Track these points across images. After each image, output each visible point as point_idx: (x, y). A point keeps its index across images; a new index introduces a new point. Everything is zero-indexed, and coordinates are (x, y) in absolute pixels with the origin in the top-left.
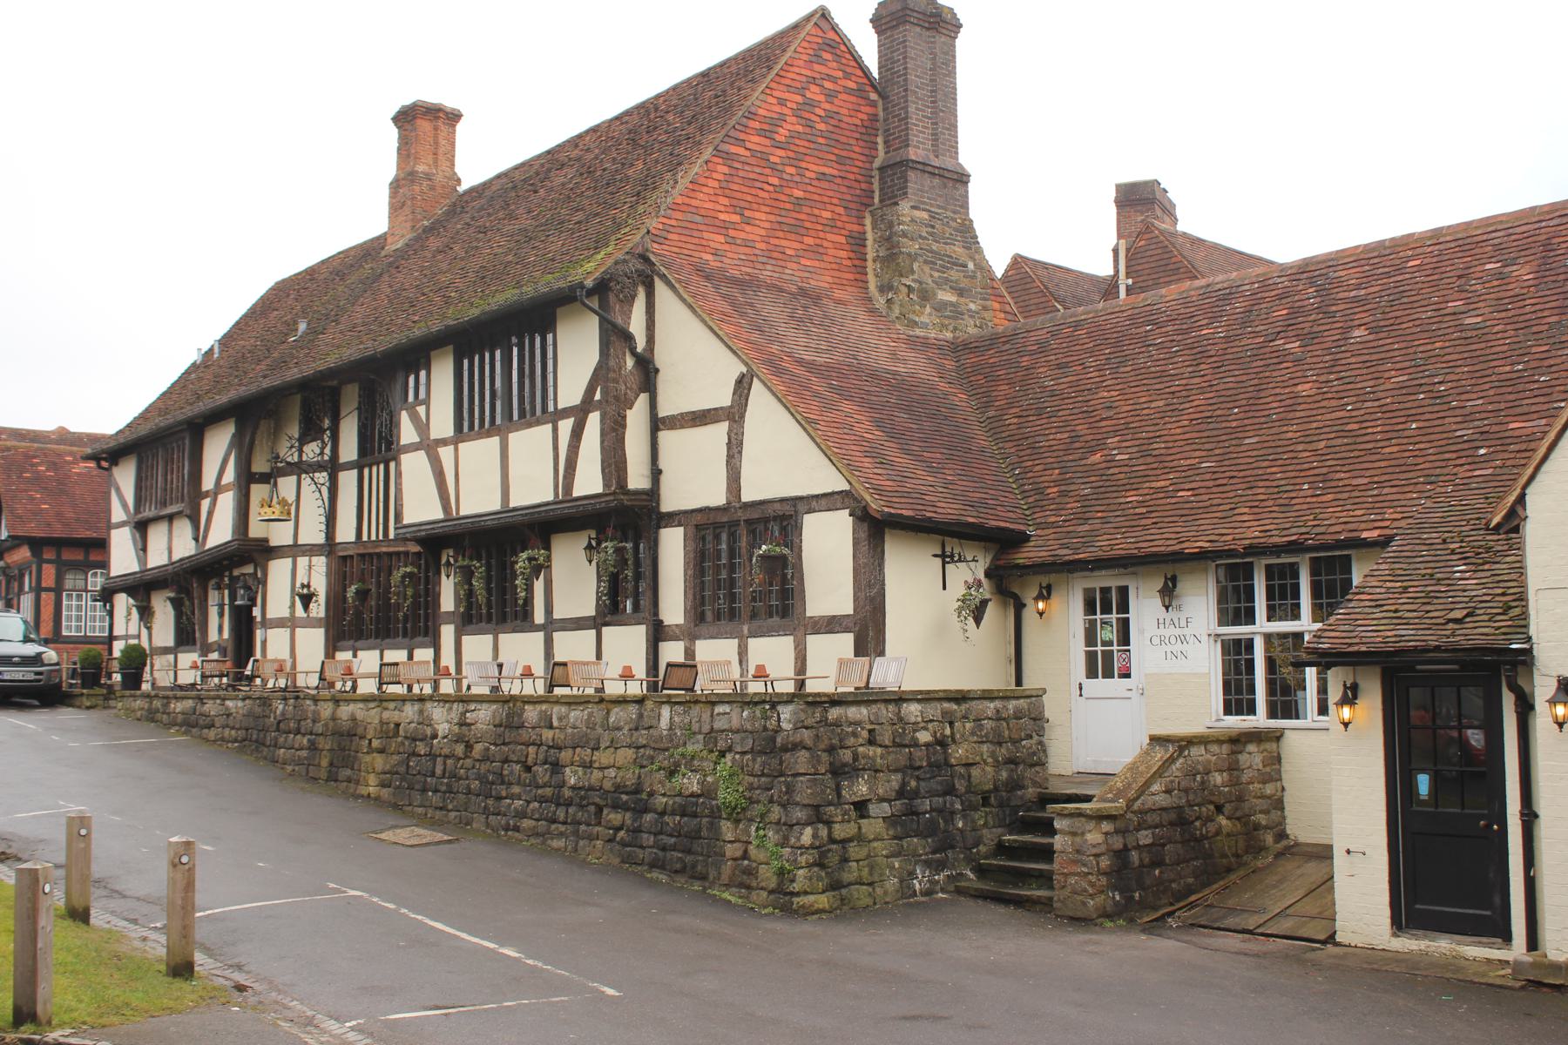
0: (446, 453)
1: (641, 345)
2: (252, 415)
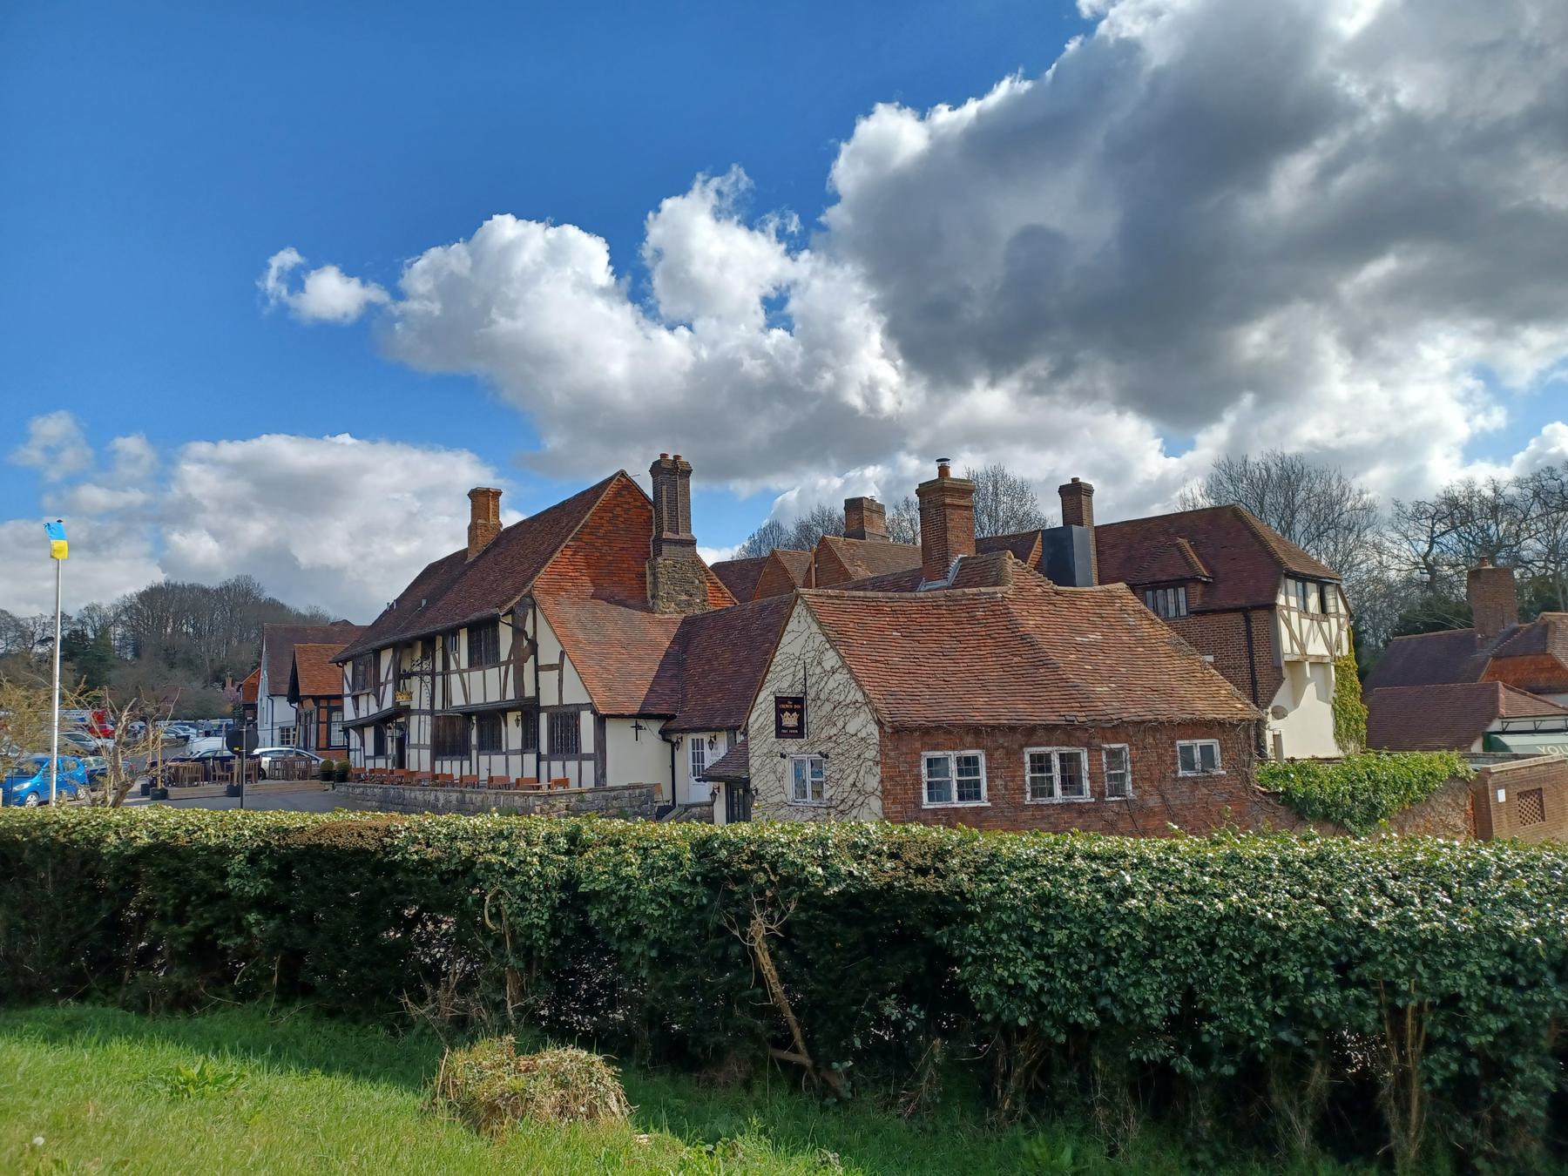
0: (465, 675)
1: (530, 635)
2: (401, 647)
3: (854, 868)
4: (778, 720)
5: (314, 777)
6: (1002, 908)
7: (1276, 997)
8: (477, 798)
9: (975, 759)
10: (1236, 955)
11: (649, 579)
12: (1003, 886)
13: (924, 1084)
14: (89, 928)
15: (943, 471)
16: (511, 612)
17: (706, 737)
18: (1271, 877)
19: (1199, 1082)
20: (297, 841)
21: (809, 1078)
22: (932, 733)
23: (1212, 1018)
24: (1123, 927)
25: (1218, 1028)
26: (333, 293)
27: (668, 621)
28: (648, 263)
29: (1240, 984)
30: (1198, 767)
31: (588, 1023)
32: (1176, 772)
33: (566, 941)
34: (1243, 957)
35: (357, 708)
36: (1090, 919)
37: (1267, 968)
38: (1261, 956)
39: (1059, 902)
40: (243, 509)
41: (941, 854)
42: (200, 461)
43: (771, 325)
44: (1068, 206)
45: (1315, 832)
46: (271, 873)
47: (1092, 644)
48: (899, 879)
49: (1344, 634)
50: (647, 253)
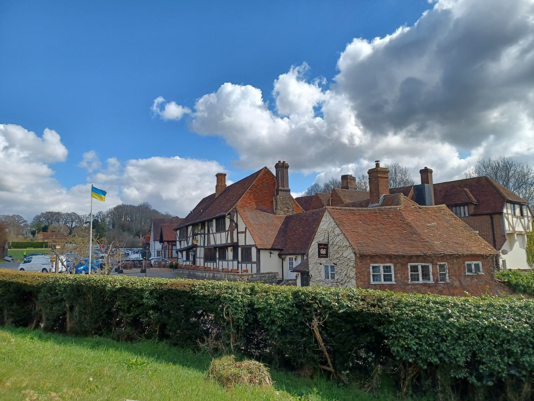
2: (194, 225)
3: (349, 303)
4: (319, 252)
5: (167, 267)
6: (402, 320)
7: (509, 357)
8: (219, 275)
9: (390, 267)
10: (493, 341)
11: (274, 203)
12: (403, 312)
13: (374, 380)
14: (103, 313)
15: (377, 165)
16: (229, 214)
17: (294, 257)
18: (506, 313)
19: (479, 387)
20: (165, 288)
21: (333, 376)
22: (374, 257)
23: (483, 363)
24: (448, 328)
25: (486, 367)
26: (174, 111)
27: (280, 218)
28: (274, 97)
29: (494, 351)
30: (474, 271)
31: (257, 353)
32: (465, 273)
33: (250, 324)
34: (495, 342)
35: (181, 245)
36: (435, 325)
37: (505, 346)
38: (503, 342)
39: (424, 318)
40: (146, 181)
41: (380, 300)
42: (133, 165)
43: (316, 116)
44: (425, 71)
45: (523, 297)
46: (156, 298)
47: (433, 226)
48: (365, 308)
49: (530, 224)
50: (274, 93)
